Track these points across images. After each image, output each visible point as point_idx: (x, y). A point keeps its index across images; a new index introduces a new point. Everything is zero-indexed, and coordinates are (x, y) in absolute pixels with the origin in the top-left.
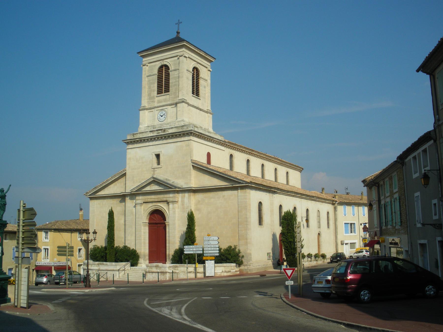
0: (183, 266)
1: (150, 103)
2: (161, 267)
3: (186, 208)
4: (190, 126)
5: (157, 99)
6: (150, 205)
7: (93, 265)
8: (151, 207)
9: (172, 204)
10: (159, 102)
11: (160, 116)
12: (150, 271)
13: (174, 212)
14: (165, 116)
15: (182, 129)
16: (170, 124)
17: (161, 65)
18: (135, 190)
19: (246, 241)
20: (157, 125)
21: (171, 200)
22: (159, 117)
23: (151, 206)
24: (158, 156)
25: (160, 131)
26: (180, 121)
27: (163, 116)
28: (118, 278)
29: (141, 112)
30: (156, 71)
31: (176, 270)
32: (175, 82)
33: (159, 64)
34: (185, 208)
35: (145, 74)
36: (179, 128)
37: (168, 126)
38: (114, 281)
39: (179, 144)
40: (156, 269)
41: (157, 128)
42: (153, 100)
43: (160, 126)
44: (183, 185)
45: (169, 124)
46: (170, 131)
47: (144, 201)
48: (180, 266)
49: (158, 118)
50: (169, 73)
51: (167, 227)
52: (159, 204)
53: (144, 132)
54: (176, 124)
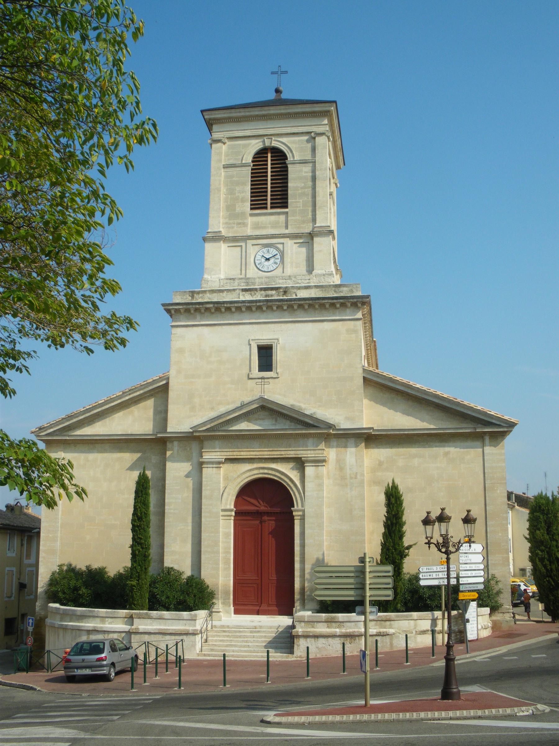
0: (407, 616)
1: (233, 227)
2: (343, 622)
3: (351, 478)
4: (357, 287)
5: (250, 220)
6: (247, 467)
7: (107, 619)
9: (314, 467)
10: (257, 226)
11: (263, 260)
12: (309, 632)
13: (321, 485)
15: (335, 291)
16: (295, 277)
17: (262, 146)
18: (204, 428)
19: (505, 555)
20: (259, 278)
22: (258, 260)
23: (250, 470)
25: (274, 292)
26: (324, 275)
27: (272, 260)
28: (198, 655)
29: (209, 247)
30: (248, 159)
31: (385, 628)
33: (256, 145)
34: (348, 477)
35: (220, 161)
36: (327, 289)
37: (291, 283)
38: (226, 663)
40: (328, 627)
41: (257, 284)
42: (240, 221)
43: (267, 280)
44: (340, 423)
45: (293, 279)
46: (303, 294)
47: (228, 457)
48: (397, 616)
49: (257, 262)
50: (287, 167)
51: (296, 521)
53: (226, 290)
54: (311, 280)
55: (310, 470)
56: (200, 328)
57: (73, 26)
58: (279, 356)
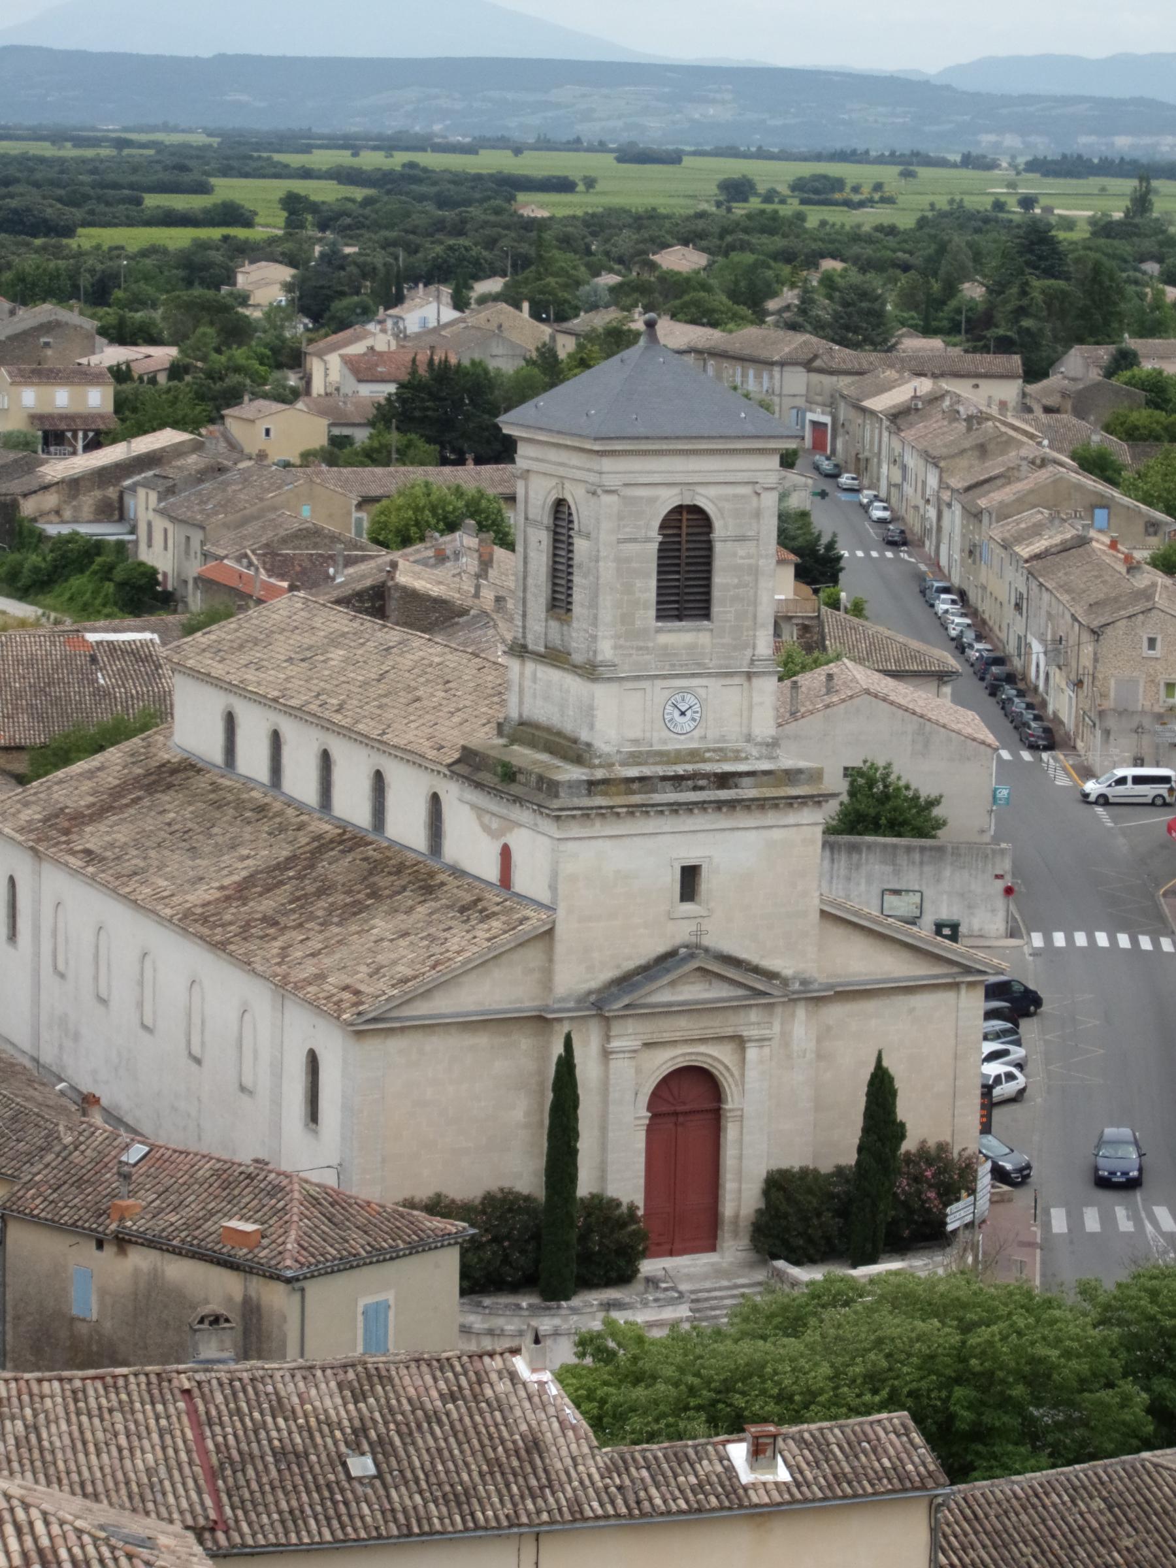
8: (663, 1062)
11: (676, 713)
14: (697, 716)
21: (754, 1032)
24: (690, 877)
27: (689, 713)
32: (737, 587)
39: (777, 834)
42: (641, 644)
49: (667, 717)
52: (702, 1049)
55: (752, 1053)
56: (600, 841)
57: (206, 503)
58: (707, 883)
